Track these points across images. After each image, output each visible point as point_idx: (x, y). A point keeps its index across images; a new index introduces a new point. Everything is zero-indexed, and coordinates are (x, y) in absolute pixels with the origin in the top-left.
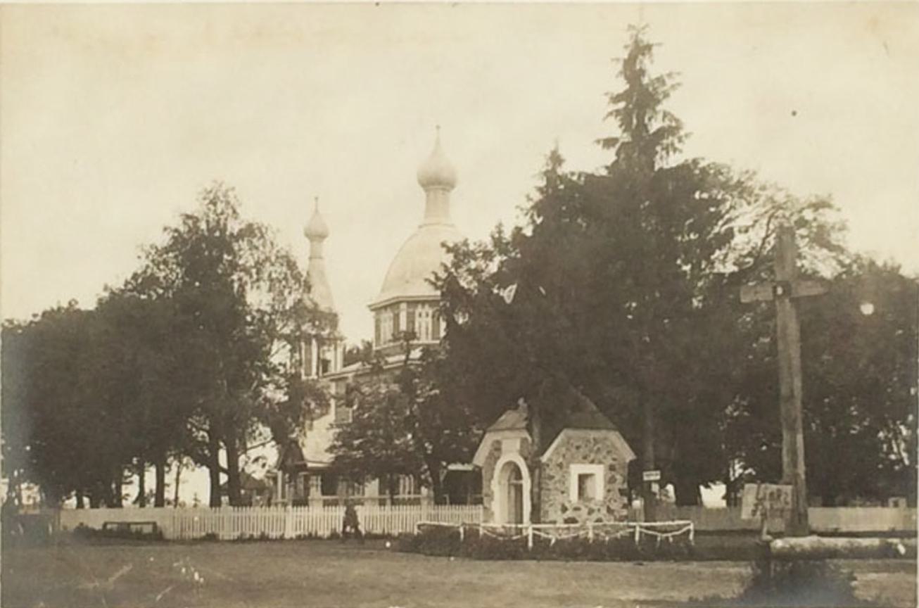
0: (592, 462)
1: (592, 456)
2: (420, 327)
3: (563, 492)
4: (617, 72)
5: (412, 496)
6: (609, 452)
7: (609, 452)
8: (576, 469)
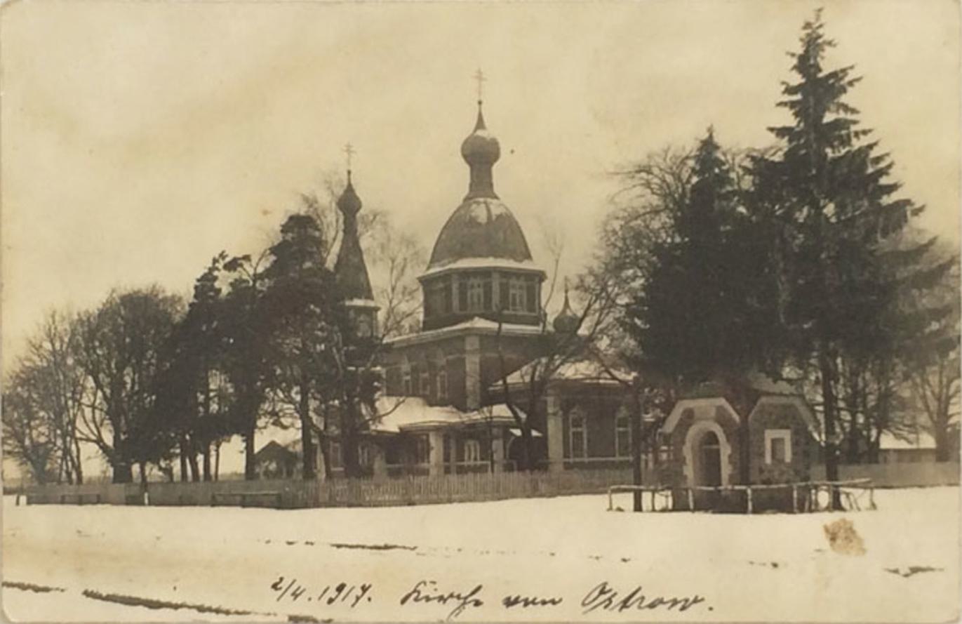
2: (472, 298)
4: (791, 65)
5: (479, 463)
8: (770, 435)
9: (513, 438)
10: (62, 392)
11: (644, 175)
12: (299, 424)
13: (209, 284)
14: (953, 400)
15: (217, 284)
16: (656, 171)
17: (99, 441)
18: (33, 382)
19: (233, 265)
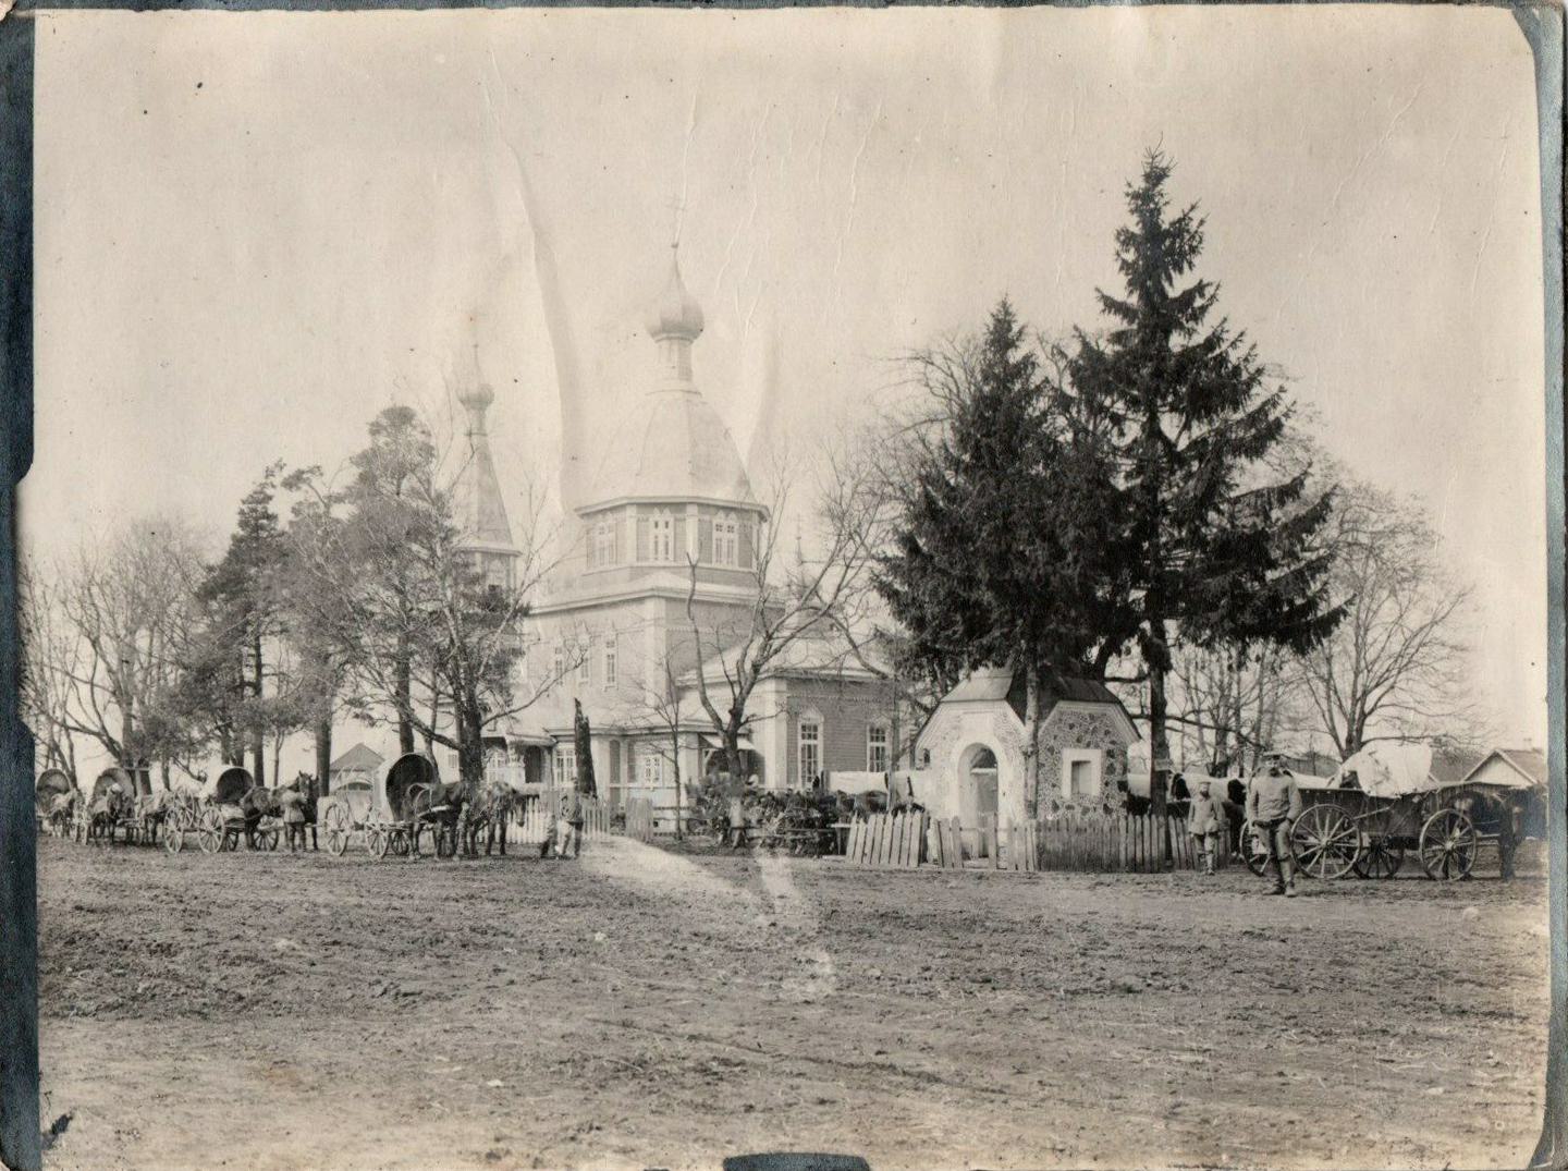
0: (1088, 745)
1: (1088, 738)
3: (1054, 786)
6: (1107, 733)
7: (1107, 733)
8: (1070, 755)
9: (711, 751)
10: (46, 660)
11: (920, 365)
12: (394, 715)
13: (260, 507)
14: (1368, 721)
15: (272, 508)
16: (938, 360)
17: (102, 733)
18: (957, 160)
19: (295, 481)
